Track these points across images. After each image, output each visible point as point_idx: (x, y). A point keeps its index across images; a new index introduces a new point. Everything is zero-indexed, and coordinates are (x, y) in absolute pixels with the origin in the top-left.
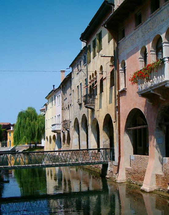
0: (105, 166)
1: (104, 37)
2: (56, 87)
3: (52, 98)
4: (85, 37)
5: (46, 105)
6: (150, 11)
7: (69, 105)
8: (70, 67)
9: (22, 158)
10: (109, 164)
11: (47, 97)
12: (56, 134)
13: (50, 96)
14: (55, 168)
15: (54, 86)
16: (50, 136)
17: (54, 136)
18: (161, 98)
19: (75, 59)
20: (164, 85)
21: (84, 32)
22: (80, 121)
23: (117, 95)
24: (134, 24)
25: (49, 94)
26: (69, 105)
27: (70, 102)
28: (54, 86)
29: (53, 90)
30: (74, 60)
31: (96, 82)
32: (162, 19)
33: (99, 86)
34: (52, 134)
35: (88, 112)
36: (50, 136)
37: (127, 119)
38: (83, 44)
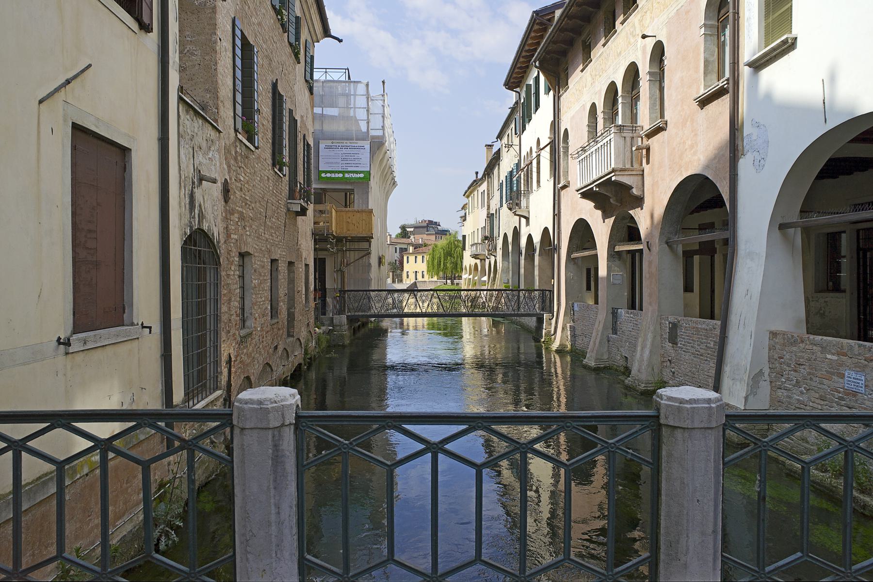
0: (540, 320)
1: (720, 149)
2: (480, 176)
4: (514, 81)
5: (464, 208)
6: (602, 34)
8: (497, 138)
9: (442, 306)
11: (466, 193)
12: (478, 261)
13: (471, 193)
15: (477, 173)
17: (476, 265)
18: (611, 200)
19: (504, 124)
22: (510, 239)
24: (580, 57)
25: (469, 188)
28: (477, 173)
29: (475, 181)
30: (503, 127)
32: (618, 52)
35: (129, 28)
38: (512, 97)
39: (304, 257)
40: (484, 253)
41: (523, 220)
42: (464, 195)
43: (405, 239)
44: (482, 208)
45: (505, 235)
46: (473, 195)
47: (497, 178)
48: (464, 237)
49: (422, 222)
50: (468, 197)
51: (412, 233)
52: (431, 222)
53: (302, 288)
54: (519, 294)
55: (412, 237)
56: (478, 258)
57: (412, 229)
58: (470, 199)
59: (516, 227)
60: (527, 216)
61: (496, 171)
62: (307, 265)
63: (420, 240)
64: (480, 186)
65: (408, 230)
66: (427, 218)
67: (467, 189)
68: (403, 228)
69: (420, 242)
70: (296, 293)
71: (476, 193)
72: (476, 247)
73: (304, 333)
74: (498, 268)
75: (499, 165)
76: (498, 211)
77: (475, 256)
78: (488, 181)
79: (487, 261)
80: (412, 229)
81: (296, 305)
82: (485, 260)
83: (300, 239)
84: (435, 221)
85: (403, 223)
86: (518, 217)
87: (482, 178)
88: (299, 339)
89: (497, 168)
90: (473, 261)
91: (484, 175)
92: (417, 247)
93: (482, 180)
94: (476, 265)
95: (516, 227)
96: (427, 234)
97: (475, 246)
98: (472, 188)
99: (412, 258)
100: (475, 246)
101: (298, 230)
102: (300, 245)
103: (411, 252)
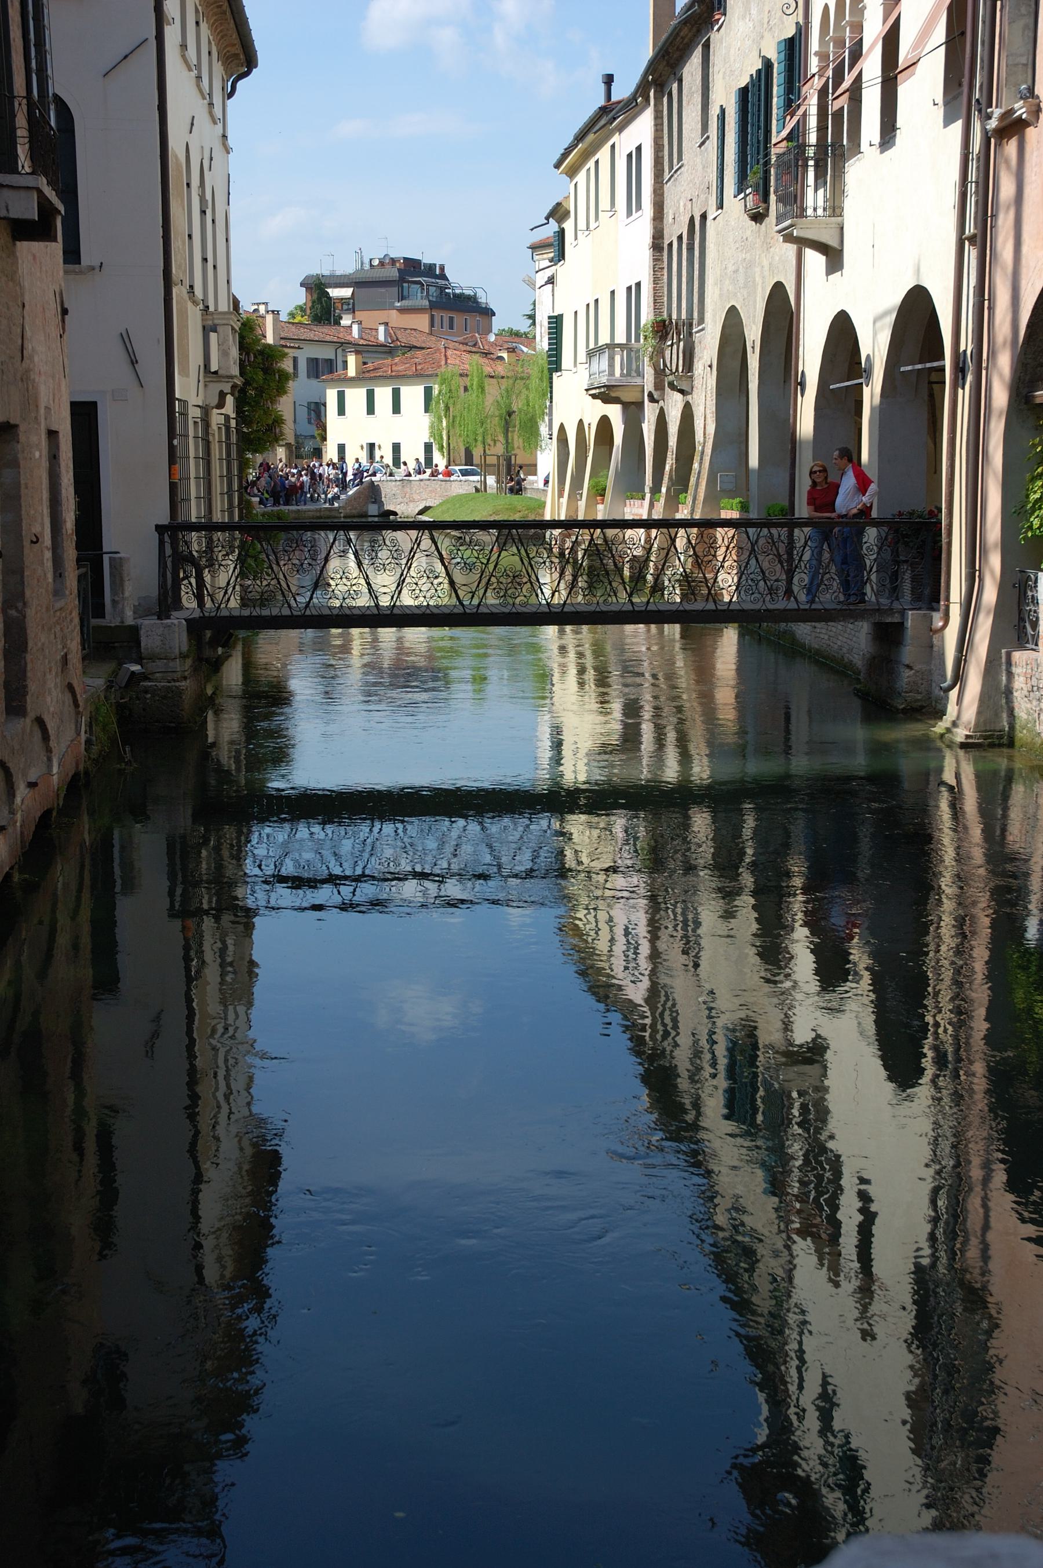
2: (622, 91)
3: (597, 162)
5: (558, 213)
7: (692, 219)
10: (909, 623)
14: (375, 640)
15: (609, 80)
16: (581, 421)
17: (605, 423)
20: (667, 1139)
21: (983, 685)
22: (753, 332)
23: (978, 101)
25: (580, 137)
26: (692, 219)
27: (703, 197)
28: (609, 80)
29: (603, 111)
31: (857, 54)
33: (879, 87)
34: (594, 411)
36: (581, 421)
37: (882, 1058)
39: (43, 403)
40: (638, 381)
41: (815, 261)
42: (557, 166)
43: (326, 329)
44: (629, 213)
45: (733, 319)
46: (591, 164)
47: (698, 99)
48: (556, 323)
49: (382, 263)
50: (572, 172)
51: (350, 306)
52: (412, 268)
53: (42, 525)
54: (791, 535)
55: (346, 321)
56: (615, 400)
57: (346, 292)
58: (581, 177)
59: (778, 288)
60: (833, 243)
61: (692, 69)
62: (52, 434)
63: (381, 329)
64: (621, 129)
65: (335, 293)
66: (399, 252)
67: (569, 139)
68: (317, 287)
69: (381, 337)
70: (27, 543)
71: (603, 155)
72: (611, 359)
73: (54, 694)
74: (699, 437)
75: (707, 46)
76: (698, 226)
77: (605, 394)
78: (658, 116)
79: (650, 412)
80: (346, 292)
81: (28, 593)
82: (640, 405)
83: (28, 333)
84: (426, 260)
85: (315, 270)
86: (791, 249)
87: (634, 98)
88: (40, 722)
89: (697, 53)
90: (594, 411)
91: (642, 88)
92: (365, 349)
93: (630, 108)
94: (605, 423)
95: (778, 288)
96: (402, 310)
97: (605, 358)
98: (591, 137)
99: (356, 397)
100: (605, 358)
101: (22, 295)
102: (31, 358)
103: (352, 372)
